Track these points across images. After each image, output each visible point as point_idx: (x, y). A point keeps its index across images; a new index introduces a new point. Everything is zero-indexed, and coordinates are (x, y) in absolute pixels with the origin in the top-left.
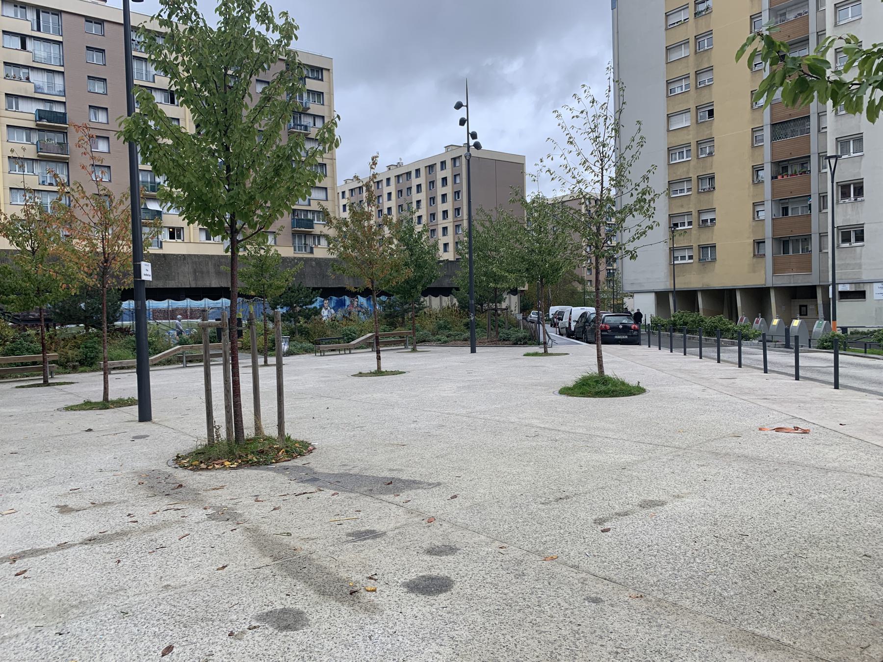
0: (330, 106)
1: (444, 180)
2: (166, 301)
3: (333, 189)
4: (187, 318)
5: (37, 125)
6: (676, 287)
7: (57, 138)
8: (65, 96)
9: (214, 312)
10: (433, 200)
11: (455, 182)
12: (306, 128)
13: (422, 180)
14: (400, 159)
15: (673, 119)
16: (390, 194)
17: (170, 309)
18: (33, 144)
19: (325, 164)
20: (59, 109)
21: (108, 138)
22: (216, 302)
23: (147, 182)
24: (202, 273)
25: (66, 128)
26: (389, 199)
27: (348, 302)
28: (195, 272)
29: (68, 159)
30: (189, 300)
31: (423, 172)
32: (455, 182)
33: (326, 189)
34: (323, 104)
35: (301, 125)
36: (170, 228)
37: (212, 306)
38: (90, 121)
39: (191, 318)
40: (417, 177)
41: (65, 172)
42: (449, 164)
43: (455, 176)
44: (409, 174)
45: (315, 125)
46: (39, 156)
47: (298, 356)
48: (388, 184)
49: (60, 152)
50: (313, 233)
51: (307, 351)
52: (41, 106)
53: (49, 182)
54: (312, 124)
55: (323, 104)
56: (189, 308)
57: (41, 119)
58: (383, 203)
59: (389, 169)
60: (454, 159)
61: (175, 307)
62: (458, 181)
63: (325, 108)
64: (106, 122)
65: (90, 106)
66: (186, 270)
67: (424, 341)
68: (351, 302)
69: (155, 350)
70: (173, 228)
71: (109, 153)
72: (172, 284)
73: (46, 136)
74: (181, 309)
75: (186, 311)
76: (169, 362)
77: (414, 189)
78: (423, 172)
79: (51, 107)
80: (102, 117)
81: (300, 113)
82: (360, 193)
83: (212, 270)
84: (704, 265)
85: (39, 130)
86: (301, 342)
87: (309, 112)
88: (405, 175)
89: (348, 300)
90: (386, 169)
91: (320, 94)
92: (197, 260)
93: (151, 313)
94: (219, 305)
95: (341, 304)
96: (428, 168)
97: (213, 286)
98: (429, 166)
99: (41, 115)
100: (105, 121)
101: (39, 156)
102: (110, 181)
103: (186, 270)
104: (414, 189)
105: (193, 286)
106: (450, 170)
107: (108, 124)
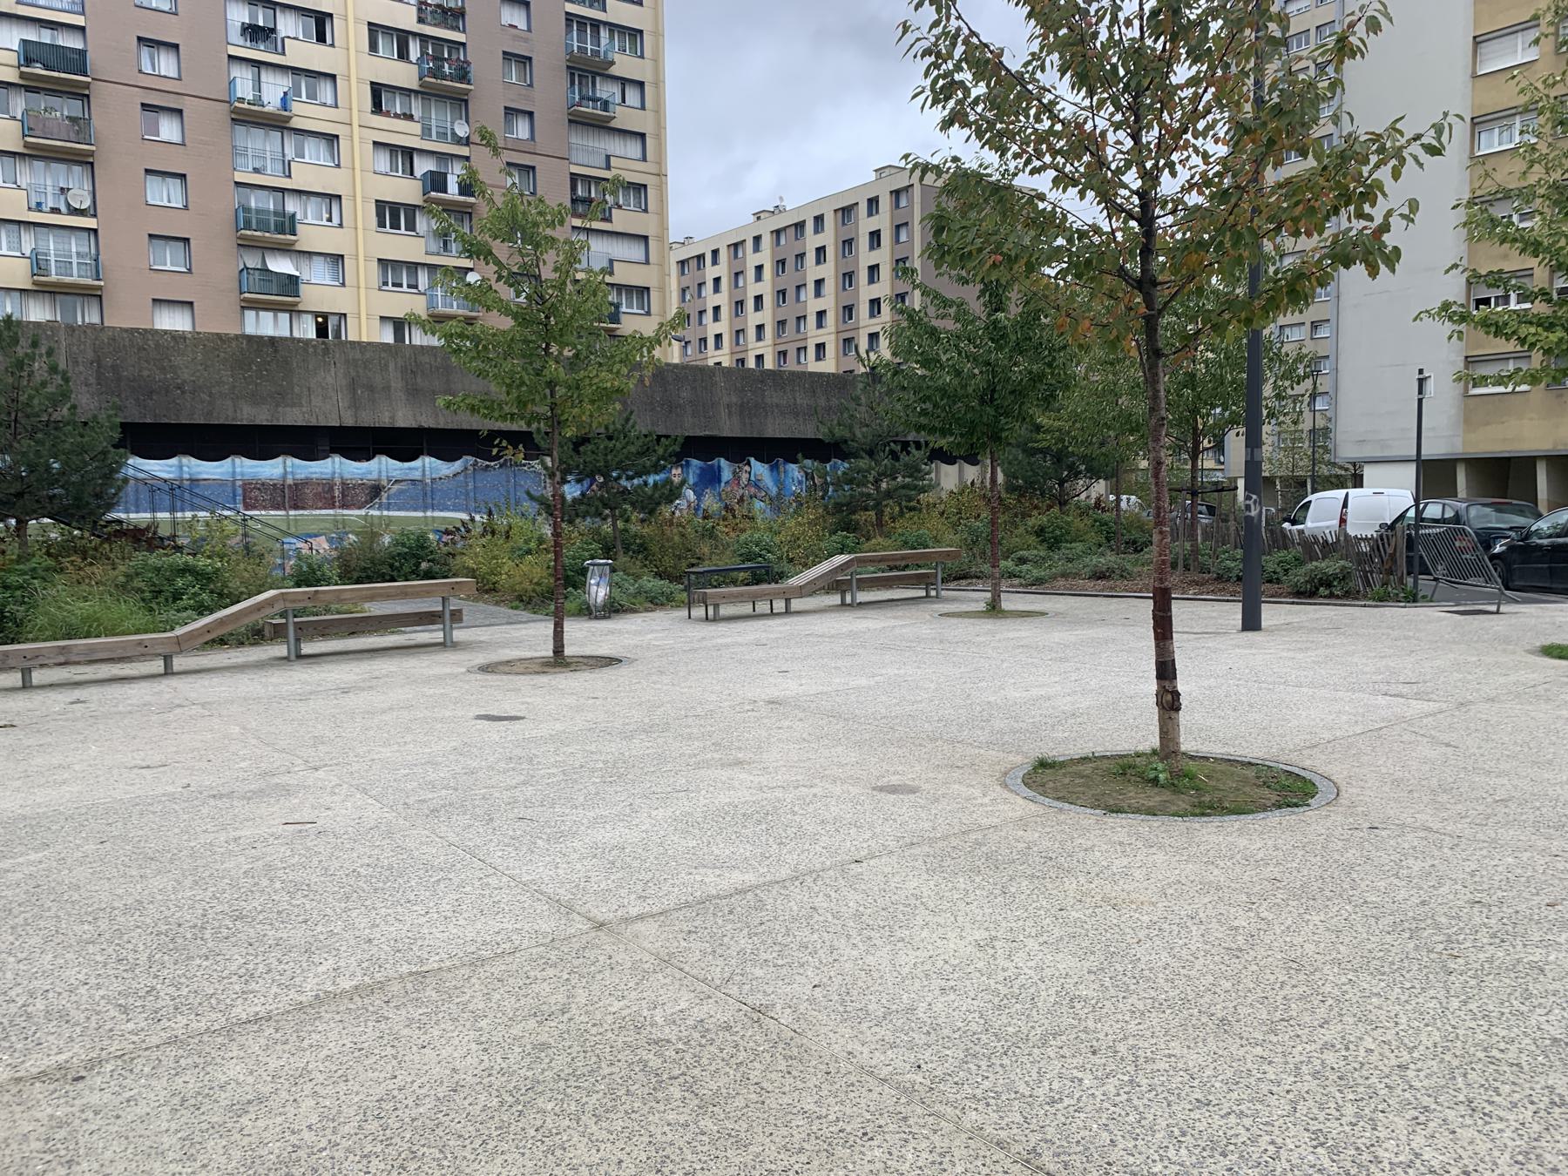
0: (657, 62)
1: (875, 236)
2: (280, 460)
3: (662, 238)
4: (333, 507)
5: (22, 75)
6: (1423, 452)
7: (72, 107)
8: (83, 13)
9: (401, 492)
10: (848, 277)
11: (897, 240)
12: (606, 105)
13: (828, 238)
14: (781, 199)
15: (1485, 48)
16: (759, 268)
17: (290, 481)
18: (14, 118)
19: (645, 186)
20: (72, 42)
21: (180, 112)
22: (407, 465)
23: (269, 211)
24: (371, 388)
25: (87, 86)
26: (759, 278)
27: (727, 474)
28: (353, 386)
29: (92, 154)
30: (337, 459)
31: (829, 222)
32: (897, 240)
33: (646, 238)
34: (642, 57)
35: (595, 100)
36: (317, 315)
37: (397, 475)
38: (140, 71)
39: (343, 506)
40: (816, 231)
41: (87, 186)
42: (885, 203)
43: (898, 227)
44: (800, 226)
45: (624, 101)
46: (27, 145)
47: (1234, 823)
48: (757, 249)
49: (73, 136)
50: (618, 333)
51: (656, 602)
52: (32, 35)
53: (51, 204)
54: (618, 99)
55: (642, 57)
56: (338, 481)
57: (29, 61)
58: (745, 287)
59: (759, 218)
60: (896, 194)
61: (301, 474)
62: (903, 238)
63: (647, 63)
64: (175, 75)
65: (140, 39)
66: (330, 380)
67: (964, 577)
68: (734, 473)
69: (221, 595)
70: (325, 316)
71: (183, 144)
72: (293, 416)
73: (43, 101)
74: (319, 482)
75: (331, 489)
76: (257, 636)
77: (811, 257)
78: (829, 222)
79: (53, 37)
80: (166, 64)
81: (595, 74)
82: (699, 269)
83: (397, 383)
84: (1561, 396)
85: (28, 89)
86: (637, 577)
87: (614, 71)
88: (793, 228)
89: (726, 468)
90: (753, 219)
91: (636, 34)
92: (358, 356)
93: (240, 491)
94: (417, 475)
95: (711, 478)
96: (840, 213)
97: (401, 424)
98: (843, 209)
99: (29, 53)
100: (173, 73)
101: (27, 145)
102: (186, 207)
103: (330, 380)
104: (811, 257)
105: (349, 422)
106: (888, 215)
107: (180, 79)
